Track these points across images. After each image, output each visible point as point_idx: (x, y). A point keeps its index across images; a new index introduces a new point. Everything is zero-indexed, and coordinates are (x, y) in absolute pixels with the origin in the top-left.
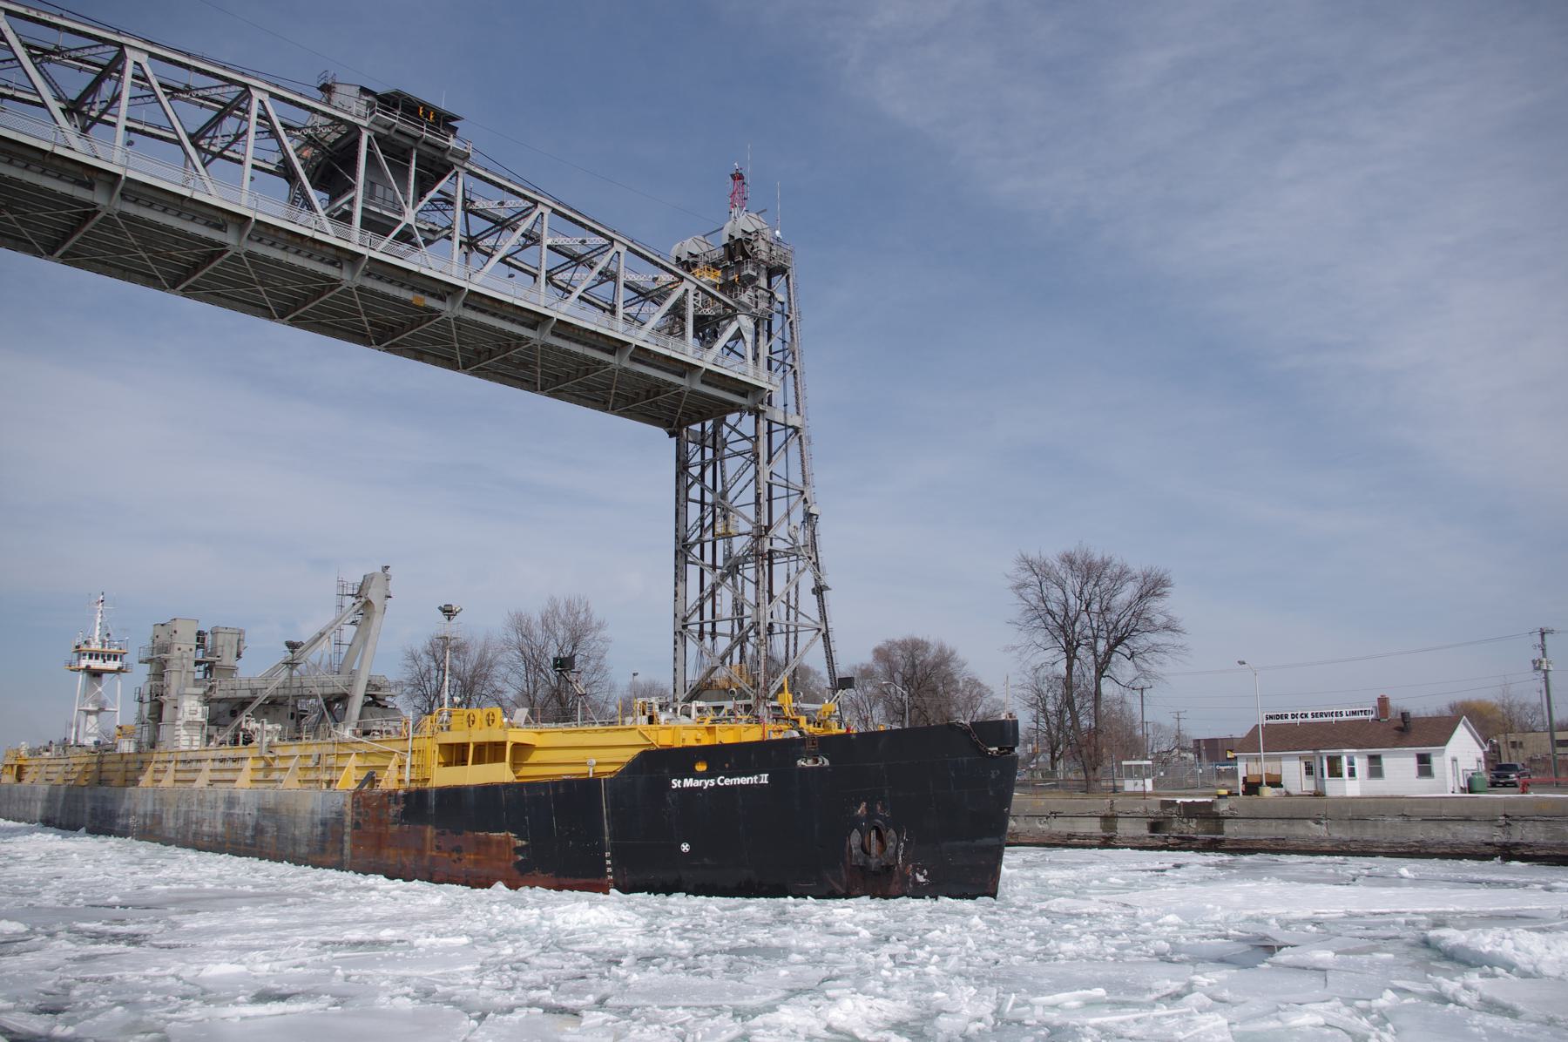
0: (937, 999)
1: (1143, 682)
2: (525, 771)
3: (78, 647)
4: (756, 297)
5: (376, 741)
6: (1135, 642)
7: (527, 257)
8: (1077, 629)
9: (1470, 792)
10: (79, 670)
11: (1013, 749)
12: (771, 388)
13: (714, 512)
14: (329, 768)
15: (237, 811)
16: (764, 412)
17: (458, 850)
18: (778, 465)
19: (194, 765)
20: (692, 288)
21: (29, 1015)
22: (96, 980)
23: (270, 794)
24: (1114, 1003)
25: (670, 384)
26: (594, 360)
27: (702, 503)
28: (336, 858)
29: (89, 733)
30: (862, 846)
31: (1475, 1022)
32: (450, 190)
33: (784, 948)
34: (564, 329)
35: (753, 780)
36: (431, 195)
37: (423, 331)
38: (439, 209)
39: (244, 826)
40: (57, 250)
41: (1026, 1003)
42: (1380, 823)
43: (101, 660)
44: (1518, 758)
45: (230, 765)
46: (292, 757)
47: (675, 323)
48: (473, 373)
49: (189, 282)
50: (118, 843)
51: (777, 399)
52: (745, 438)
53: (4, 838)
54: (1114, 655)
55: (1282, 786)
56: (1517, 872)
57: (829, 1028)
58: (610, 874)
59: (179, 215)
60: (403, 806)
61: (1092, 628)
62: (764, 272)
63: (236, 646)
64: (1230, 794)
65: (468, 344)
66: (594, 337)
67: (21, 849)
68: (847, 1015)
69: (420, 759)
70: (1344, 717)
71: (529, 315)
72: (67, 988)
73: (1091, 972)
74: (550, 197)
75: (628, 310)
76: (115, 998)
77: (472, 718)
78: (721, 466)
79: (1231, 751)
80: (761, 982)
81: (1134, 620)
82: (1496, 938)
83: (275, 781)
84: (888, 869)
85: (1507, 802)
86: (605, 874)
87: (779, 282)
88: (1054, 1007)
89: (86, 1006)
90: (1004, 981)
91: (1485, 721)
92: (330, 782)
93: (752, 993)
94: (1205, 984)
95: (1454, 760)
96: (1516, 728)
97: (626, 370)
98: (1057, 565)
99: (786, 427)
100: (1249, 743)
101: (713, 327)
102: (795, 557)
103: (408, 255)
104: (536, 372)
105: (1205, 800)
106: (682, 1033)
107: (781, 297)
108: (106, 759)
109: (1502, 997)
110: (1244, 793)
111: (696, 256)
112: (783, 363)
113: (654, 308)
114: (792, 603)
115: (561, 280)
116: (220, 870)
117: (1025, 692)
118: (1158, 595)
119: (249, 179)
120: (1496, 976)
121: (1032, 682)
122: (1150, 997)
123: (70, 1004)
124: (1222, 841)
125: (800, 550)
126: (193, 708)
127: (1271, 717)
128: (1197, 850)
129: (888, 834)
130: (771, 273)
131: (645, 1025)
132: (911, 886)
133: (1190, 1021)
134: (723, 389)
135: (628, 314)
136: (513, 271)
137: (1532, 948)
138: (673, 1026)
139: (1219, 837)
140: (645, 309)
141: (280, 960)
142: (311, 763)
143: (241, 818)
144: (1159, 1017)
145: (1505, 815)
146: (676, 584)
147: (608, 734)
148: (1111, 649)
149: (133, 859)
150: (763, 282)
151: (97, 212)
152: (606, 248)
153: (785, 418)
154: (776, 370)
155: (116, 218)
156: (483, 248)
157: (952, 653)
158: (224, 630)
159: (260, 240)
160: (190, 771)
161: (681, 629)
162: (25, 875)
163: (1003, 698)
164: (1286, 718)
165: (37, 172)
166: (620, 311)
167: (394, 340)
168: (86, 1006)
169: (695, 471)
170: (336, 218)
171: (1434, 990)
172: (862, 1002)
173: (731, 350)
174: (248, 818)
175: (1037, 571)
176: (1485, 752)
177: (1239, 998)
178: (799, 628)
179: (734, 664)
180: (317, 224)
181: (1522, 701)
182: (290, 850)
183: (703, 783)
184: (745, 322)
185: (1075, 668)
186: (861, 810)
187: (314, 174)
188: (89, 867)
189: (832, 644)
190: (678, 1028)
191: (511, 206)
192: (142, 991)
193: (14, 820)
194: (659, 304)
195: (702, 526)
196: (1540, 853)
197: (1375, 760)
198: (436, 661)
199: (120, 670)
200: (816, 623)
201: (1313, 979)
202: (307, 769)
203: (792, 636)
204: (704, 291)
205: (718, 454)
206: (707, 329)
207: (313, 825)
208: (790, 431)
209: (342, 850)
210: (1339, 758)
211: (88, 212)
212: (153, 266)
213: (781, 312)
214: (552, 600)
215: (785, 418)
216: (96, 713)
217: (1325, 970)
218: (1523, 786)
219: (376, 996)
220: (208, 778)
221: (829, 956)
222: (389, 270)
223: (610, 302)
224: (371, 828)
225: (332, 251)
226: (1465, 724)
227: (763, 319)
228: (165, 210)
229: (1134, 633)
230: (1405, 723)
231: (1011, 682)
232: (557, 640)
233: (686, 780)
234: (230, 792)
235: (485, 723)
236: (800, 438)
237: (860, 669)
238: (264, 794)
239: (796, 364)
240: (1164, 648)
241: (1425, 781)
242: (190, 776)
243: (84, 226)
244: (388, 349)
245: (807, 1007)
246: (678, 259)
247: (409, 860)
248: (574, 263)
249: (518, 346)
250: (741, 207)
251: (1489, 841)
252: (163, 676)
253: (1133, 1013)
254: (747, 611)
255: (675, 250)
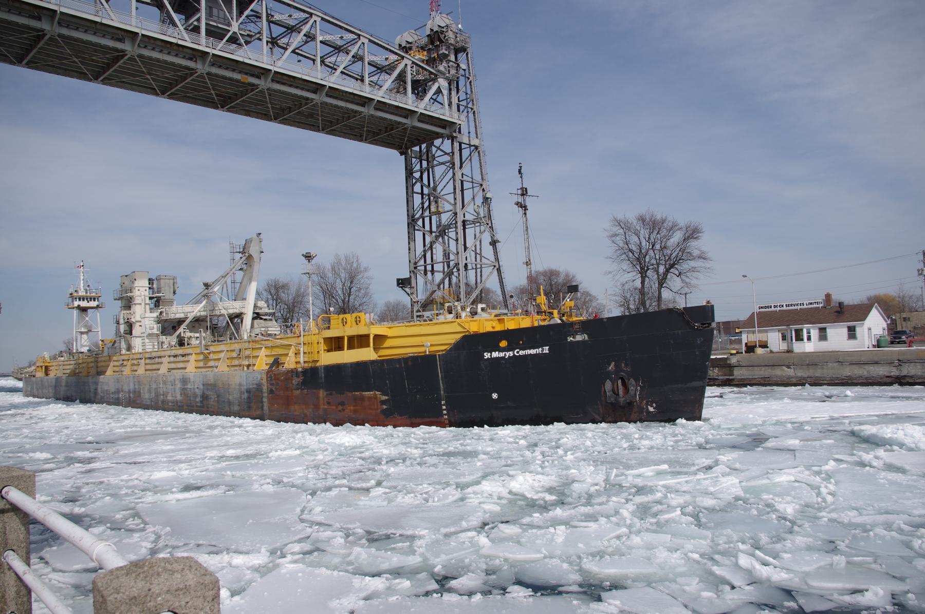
0: (572, 473)
1: (686, 290)
2: (383, 352)
3: (71, 294)
4: (449, 67)
5: (278, 339)
6: (681, 267)
7: (308, 49)
8: (647, 260)
9: (878, 347)
10: (74, 308)
11: (710, 324)
12: (460, 122)
13: (429, 199)
14: (248, 357)
15: (189, 386)
16: (456, 137)
17: (342, 404)
18: (466, 169)
19: (157, 360)
20: (409, 63)
21: (60, 503)
22: (94, 483)
23: (210, 375)
24: (673, 472)
25: (399, 123)
26: (352, 110)
27: (422, 194)
28: (259, 412)
29: (83, 345)
30: (613, 391)
31: (881, 477)
32: (258, 9)
33: (475, 452)
34: (334, 92)
35: (539, 351)
36: (247, 13)
37: (249, 98)
38: (252, 22)
39: (195, 396)
40: (24, 60)
41: (623, 474)
42: (825, 367)
43: (86, 301)
44: (907, 327)
45: (181, 358)
46: (223, 351)
47: (400, 85)
48: (281, 122)
49: (106, 75)
50: (98, 407)
51: (464, 130)
52: (446, 154)
53: (34, 408)
54: (669, 274)
55: (768, 347)
56: (917, 391)
57: (510, 492)
58: (445, 415)
59: (95, 34)
60: (302, 378)
61: (656, 259)
62: (452, 51)
63: (172, 286)
64: (737, 353)
65: (276, 105)
66: (352, 96)
67: (44, 413)
68: (521, 485)
69: (309, 348)
70: (805, 306)
71: (312, 85)
72: (79, 488)
73: (659, 456)
74: (320, 11)
75: (371, 79)
76: (106, 492)
77: (345, 320)
78: (433, 172)
79: (738, 328)
80: (467, 470)
81: (680, 253)
82: (894, 430)
83: (212, 367)
84: (630, 404)
85: (899, 353)
86: (442, 415)
87: (462, 56)
88: (639, 476)
89: (90, 498)
90: (609, 462)
91: (888, 306)
92: (248, 366)
93: (464, 475)
94: (726, 460)
95: (870, 329)
96: (907, 309)
97: (372, 116)
98: (635, 222)
99: (470, 146)
100: (749, 323)
101: (423, 87)
102: (479, 224)
103: (236, 51)
104: (318, 120)
105: (723, 357)
106: (426, 498)
107: (463, 66)
108: (100, 359)
109: (897, 462)
110: (746, 352)
111: (411, 43)
112: (466, 107)
113: (387, 76)
114: (478, 251)
115: (330, 62)
116: (158, 420)
117: (617, 298)
118: (696, 238)
119: (135, 8)
120: (894, 451)
121: (621, 292)
122: (694, 469)
123: (81, 496)
124: (733, 380)
125: (481, 220)
126: (151, 326)
127: (762, 308)
128: (719, 385)
129: (630, 382)
130: (457, 51)
131: (406, 495)
132: (645, 414)
133: (717, 481)
134: (431, 124)
135: (371, 81)
136: (300, 58)
137: (914, 434)
138: (421, 494)
139: (731, 377)
140: (382, 77)
141: (196, 467)
142: (234, 355)
143: (192, 391)
144: (699, 480)
145: (899, 360)
146: (409, 243)
147: (437, 326)
148: (667, 271)
149: (107, 415)
150: (452, 58)
151: (45, 35)
152: (356, 41)
153: (469, 140)
154: (463, 111)
155: (57, 38)
156: (281, 45)
157: (574, 277)
158: (164, 277)
159: (145, 47)
160: (154, 364)
161: (413, 269)
162: (48, 427)
163: (604, 302)
164: (771, 308)
165: (5, 12)
166: (367, 80)
167: (232, 104)
168: (90, 498)
169: (417, 175)
170: (190, 31)
171: (858, 460)
172: (529, 477)
173: (435, 100)
174: (197, 390)
175: (623, 226)
176: (888, 324)
177: (745, 467)
178: (483, 266)
179: (445, 288)
180: (179, 35)
181: (911, 294)
182: (227, 409)
183: (505, 354)
184: (442, 83)
185: (646, 283)
186: (612, 367)
187: (174, 4)
188: (83, 421)
189: (502, 274)
190: (424, 495)
191: (296, 17)
192: (121, 488)
193: (38, 397)
194: (390, 74)
195: (423, 208)
196: (918, 381)
197: (823, 331)
198: (271, 295)
199: (98, 307)
200: (493, 262)
201: (788, 456)
202: (232, 358)
203: (479, 270)
204: (417, 65)
205: (430, 164)
206: (420, 88)
207: (242, 393)
208: (472, 148)
209: (262, 407)
210: (802, 330)
211: (39, 35)
212: (82, 67)
213: (464, 76)
214: (337, 256)
215: (469, 140)
216: (87, 333)
217: (794, 450)
218: (910, 343)
219: (252, 485)
220: (167, 368)
221: (504, 454)
222: (225, 61)
223: (360, 74)
224: (281, 393)
225: (190, 52)
226: (876, 308)
227: (454, 80)
228: (86, 31)
229: (681, 261)
230: (841, 308)
231: (608, 293)
232: (341, 279)
233: (493, 353)
234: (183, 375)
235: (354, 323)
236: (479, 152)
237: (520, 289)
238: (206, 375)
239: (475, 108)
240: (699, 269)
241: (852, 342)
242: (155, 367)
243: (38, 43)
244: (229, 110)
245: (498, 481)
246: (400, 45)
247: (309, 412)
248: (337, 51)
249: (306, 104)
250: (437, 11)
251: (888, 375)
252: (130, 307)
253: (684, 478)
254: (452, 257)
255: (398, 40)
